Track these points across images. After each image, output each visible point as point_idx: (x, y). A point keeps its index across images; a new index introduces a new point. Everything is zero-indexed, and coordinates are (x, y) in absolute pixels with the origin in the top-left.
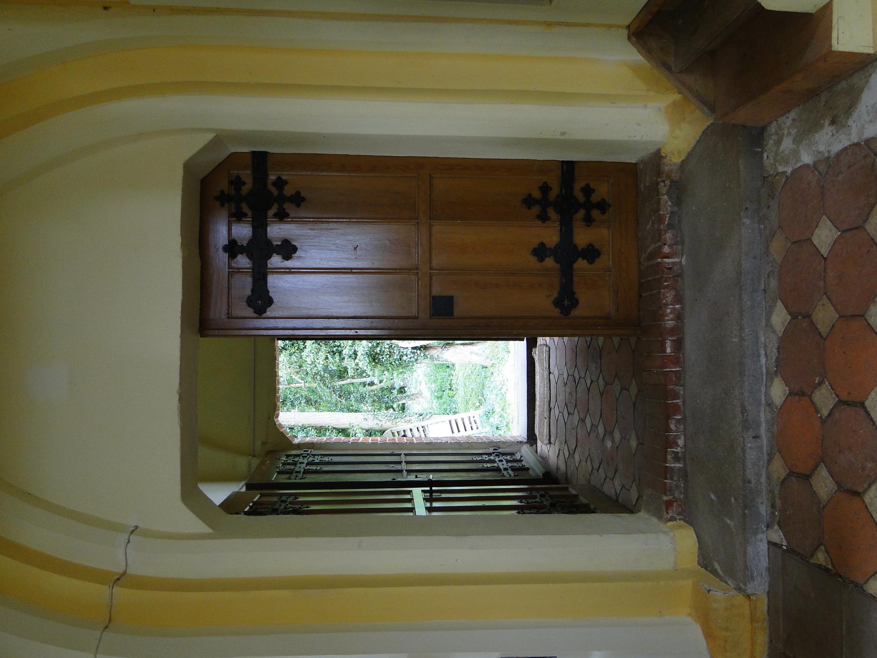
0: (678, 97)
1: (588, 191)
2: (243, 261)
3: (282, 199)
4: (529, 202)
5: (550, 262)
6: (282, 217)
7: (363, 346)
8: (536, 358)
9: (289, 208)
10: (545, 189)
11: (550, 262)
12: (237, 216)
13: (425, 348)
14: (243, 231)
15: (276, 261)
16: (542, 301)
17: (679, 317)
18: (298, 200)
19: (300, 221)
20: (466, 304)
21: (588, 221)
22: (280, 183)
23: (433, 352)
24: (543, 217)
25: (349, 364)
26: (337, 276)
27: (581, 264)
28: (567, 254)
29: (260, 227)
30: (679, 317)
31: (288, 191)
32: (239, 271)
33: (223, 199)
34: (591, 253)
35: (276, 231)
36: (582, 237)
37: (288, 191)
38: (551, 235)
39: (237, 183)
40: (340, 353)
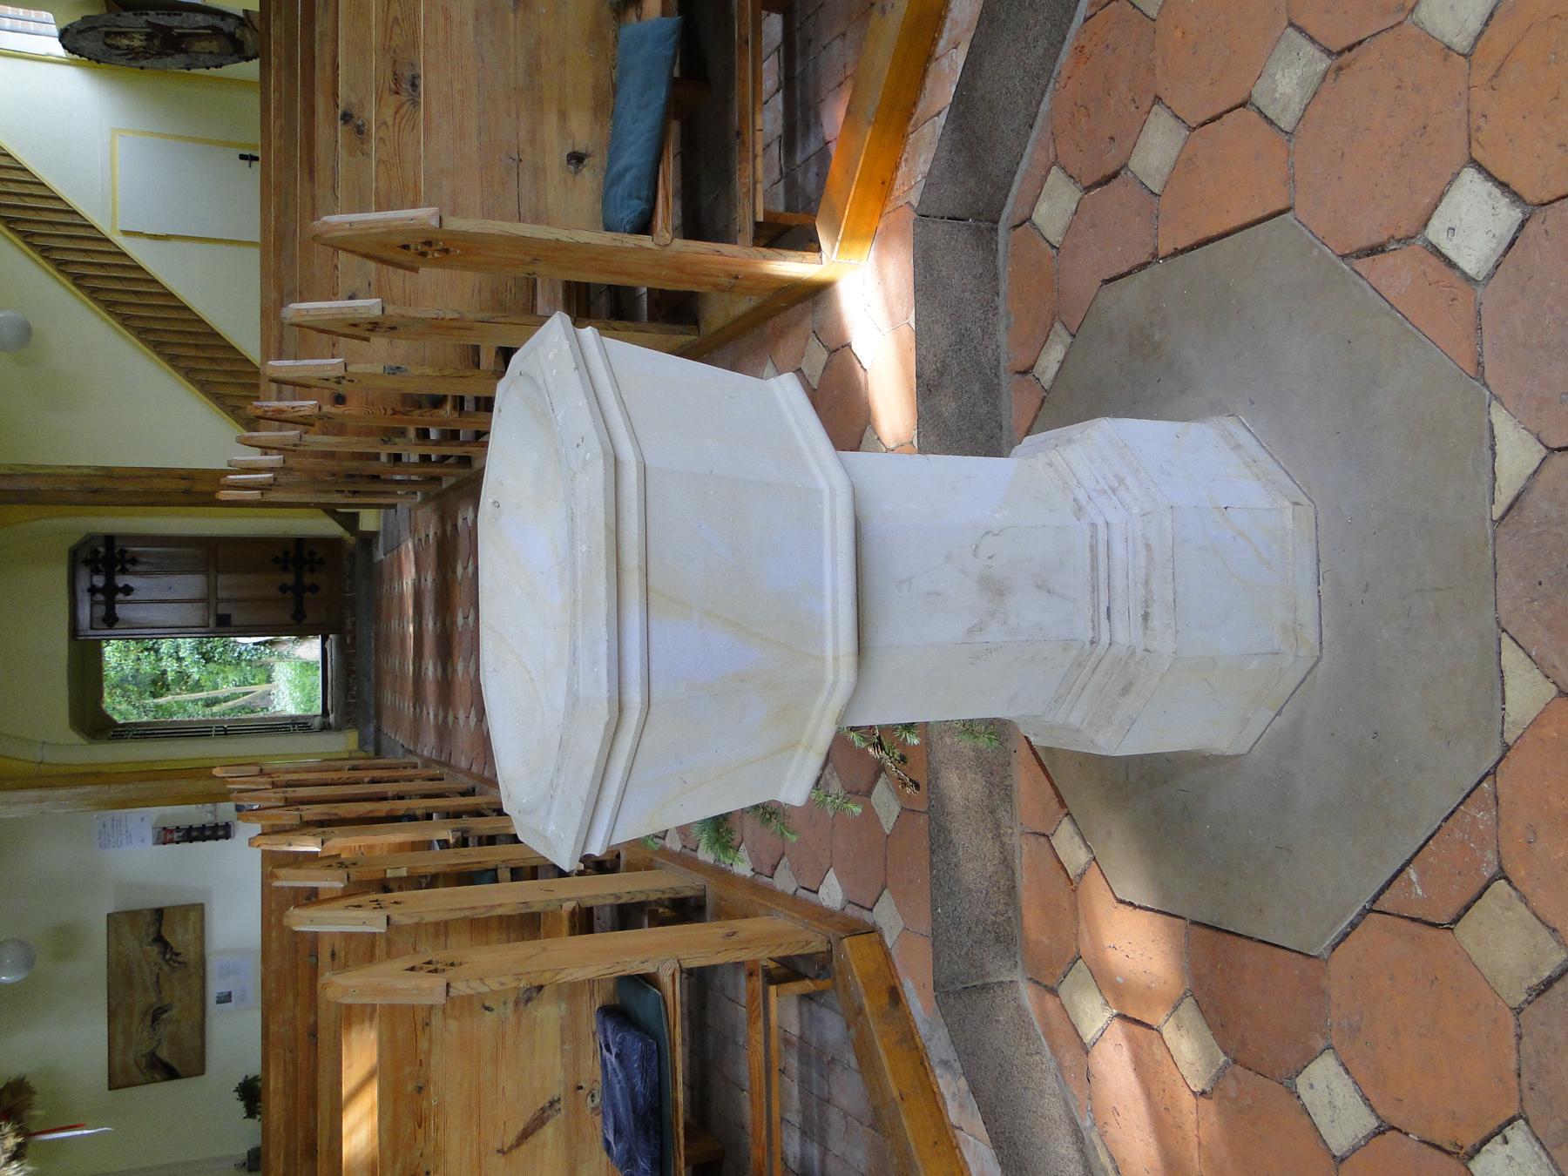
0: (770, 364)
1: (311, 553)
2: (100, 597)
3: (123, 562)
4: (276, 560)
5: (289, 594)
6: (124, 571)
7: (186, 645)
8: (580, 642)
9: (128, 566)
10: (286, 553)
11: (289, 594)
12: (96, 571)
13: (272, 643)
14: (99, 581)
15: (120, 596)
16: (286, 616)
17: (354, 624)
18: (134, 561)
19: (136, 573)
20: (237, 618)
21: (312, 570)
22: (123, 552)
23: (284, 649)
24: (285, 569)
25: (170, 666)
26: (600, 516)
27: (308, 595)
28: (299, 590)
29: (110, 578)
30: (354, 624)
31: (127, 557)
32: (99, 603)
33: (86, 562)
34: (314, 588)
35: (121, 581)
36: (308, 579)
37: (127, 557)
38: (289, 579)
39: (96, 552)
40: (157, 651)
